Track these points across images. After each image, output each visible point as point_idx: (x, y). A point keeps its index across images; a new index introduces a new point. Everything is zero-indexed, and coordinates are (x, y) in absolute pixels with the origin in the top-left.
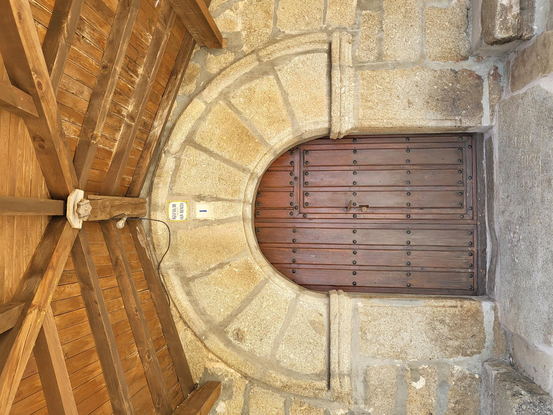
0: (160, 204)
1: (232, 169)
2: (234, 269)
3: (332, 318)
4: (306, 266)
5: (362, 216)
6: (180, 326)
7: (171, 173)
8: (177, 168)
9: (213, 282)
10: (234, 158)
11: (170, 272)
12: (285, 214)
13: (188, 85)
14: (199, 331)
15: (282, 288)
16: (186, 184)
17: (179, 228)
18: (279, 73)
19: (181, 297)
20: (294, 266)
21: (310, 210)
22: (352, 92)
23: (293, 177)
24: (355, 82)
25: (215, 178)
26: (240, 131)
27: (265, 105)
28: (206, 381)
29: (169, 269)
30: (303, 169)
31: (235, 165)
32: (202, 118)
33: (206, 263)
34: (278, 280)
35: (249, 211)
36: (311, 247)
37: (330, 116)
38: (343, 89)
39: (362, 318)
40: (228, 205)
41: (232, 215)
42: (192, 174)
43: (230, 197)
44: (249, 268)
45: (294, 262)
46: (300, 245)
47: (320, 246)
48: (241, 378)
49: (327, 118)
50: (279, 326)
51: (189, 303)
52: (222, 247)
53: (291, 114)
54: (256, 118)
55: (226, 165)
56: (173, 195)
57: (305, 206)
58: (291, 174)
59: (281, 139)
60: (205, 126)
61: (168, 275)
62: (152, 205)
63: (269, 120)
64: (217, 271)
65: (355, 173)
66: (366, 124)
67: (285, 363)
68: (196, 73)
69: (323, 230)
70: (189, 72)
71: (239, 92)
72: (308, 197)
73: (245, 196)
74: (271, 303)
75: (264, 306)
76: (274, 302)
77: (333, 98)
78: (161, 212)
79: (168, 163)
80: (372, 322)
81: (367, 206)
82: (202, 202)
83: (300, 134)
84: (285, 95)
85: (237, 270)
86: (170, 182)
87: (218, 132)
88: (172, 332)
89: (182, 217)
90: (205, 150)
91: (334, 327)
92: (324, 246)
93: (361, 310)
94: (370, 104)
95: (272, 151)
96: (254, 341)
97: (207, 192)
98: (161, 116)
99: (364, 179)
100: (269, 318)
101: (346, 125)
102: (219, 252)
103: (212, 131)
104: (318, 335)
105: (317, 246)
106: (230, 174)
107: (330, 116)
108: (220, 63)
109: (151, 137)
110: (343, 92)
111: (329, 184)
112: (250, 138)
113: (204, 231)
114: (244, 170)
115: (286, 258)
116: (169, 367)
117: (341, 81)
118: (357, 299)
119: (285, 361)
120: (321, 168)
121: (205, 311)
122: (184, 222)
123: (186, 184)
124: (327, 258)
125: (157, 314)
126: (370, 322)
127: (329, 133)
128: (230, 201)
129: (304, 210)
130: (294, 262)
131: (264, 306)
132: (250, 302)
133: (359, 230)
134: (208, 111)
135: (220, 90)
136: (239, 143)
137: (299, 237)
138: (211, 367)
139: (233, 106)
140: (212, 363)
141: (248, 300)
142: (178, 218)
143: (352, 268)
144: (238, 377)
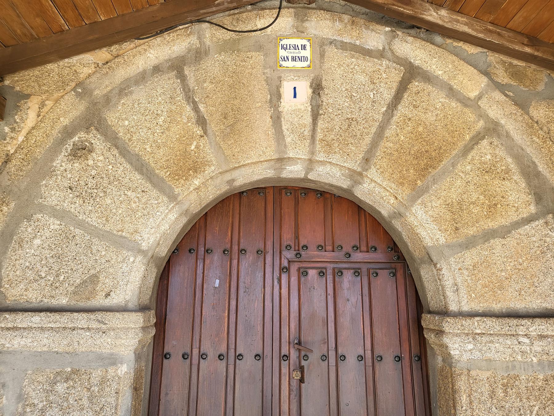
0: (306, 24)
1: (368, 140)
2: (195, 143)
3: (99, 316)
4: (200, 271)
5: (285, 370)
6: (103, 54)
7: (358, 43)
8: (367, 53)
9: (174, 108)
10: (386, 145)
11: (193, 40)
12: (288, 237)
13: (506, 71)
14: (90, 83)
15: (159, 225)
16: (339, 65)
17: (266, 55)
18: (541, 221)
19: (151, 56)
20: (202, 250)
21: (294, 279)
22: (519, 358)
23: (350, 250)
24: (540, 362)
25: (352, 112)
26: (433, 154)
27: (482, 197)
28: (6, 97)
29: (199, 38)
30: (364, 268)
31: (374, 145)
32: (451, 92)
33: (208, 96)
34: (173, 218)
35: (294, 171)
36: (231, 280)
37: (472, 315)
38: (526, 340)
39: (96, 375)
40: (306, 133)
41: (288, 140)
42: (357, 76)
43: (319, 135)
44: (196, 168)
45: (207, 251)
46: (235, 262)
47: (233, 296)
48: (7, 155)
49: (466, 308)
50: (94, 220)
51: (141, 69)
52: (234, 124)
53: (469, 244)
54: (458, 182)
55: (373, 130)
56: (321, 47)
57: (302, 270)
58: (356, 248)
59: (423, 225)
60: (439, 98)
61: (189, 35)
62: (304, 10)
63: (455, 204)
64: (192, 114)
65: (361, 358)
66: (462, 384)
67: (26, 229)
68: (527, 84)
69: (258, 294)
70: (529, 72)
71: (501, 152)
72: (316, 276)
73: (323, 163)
74: (134, 205)
75: (129, 193)
76: (134, 211)
77: (507, 320)
78: (293, 26)
79: (375, 37)
80: (86, 394)
81: (302, 380)
82: (310, 91)
83: (435, 259)
84: (504, 232)
85: (193, 147)
86: (342, 42)
87: (430, 117)
88: (91, 38)
89: (285, 59)
90: (398, 98)
91: (81, 320)
92: (233, 303)
93: (111, 371)
94: (500, 393)
95: (402, 210)
96: (69, 176)
97: (326, 99)
98: (458, 21)
99: (352, 376)
100: (109, 201)
101: (457, 346)
102: (225, 118)
103: (429, 108)
104: (71, 289)
105: (233, 290)
106: (359, 136)
107: (472, 315)
108: (548, 122)
109: (421, 5)
110: (521, 339)
111: (340, 312)
112: (423, 172)
113: (261, 94)
114: (367, 160)
115: (214, 237)
116: (29, 27)
117: (542, 337)
118: (132, 364)
119: (29, 230)
120: (366, 299)
121: (126, 95)
122: (276, 62)
123: (339, 65)
124: (213, 308)
125: (123, 15)
126: (89, 389)
127: (430, 312)
128: (313, 137)
129: (294, 269)
130: (207, 251)
131: (129, 193)
132: (136, 170)
133: (261, 366)
134: (465, 102)
135: (503, 122)
136: (412, 152)
137: (247, 262)
138: (30, 104)
139: (477, 143)
140: (37, 106)
141: (141, 167)
142: (282, 53)
143: (195, 352)
144: (9, 148)
